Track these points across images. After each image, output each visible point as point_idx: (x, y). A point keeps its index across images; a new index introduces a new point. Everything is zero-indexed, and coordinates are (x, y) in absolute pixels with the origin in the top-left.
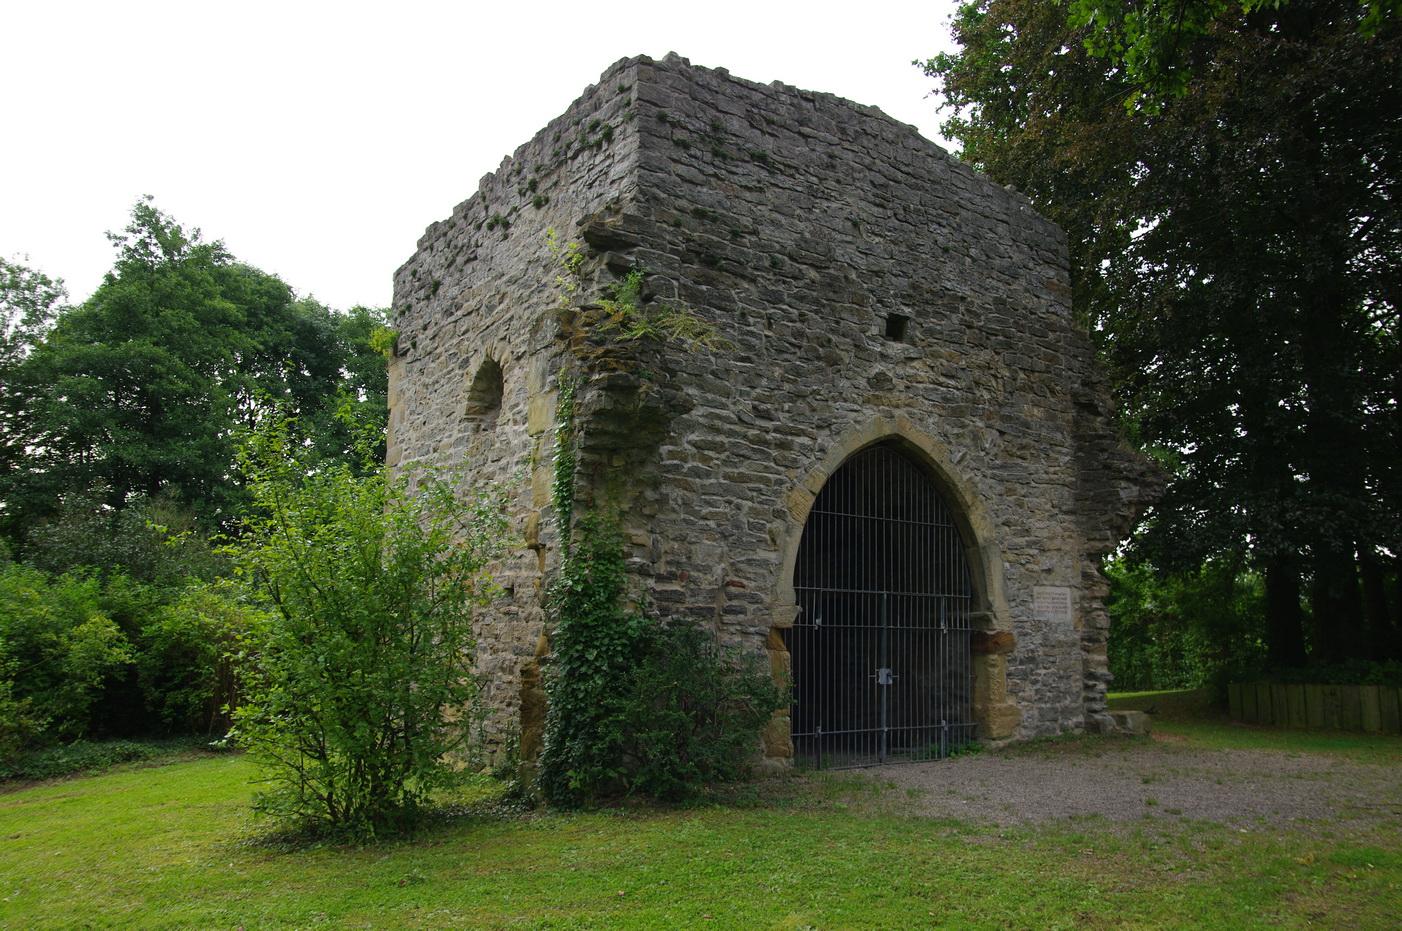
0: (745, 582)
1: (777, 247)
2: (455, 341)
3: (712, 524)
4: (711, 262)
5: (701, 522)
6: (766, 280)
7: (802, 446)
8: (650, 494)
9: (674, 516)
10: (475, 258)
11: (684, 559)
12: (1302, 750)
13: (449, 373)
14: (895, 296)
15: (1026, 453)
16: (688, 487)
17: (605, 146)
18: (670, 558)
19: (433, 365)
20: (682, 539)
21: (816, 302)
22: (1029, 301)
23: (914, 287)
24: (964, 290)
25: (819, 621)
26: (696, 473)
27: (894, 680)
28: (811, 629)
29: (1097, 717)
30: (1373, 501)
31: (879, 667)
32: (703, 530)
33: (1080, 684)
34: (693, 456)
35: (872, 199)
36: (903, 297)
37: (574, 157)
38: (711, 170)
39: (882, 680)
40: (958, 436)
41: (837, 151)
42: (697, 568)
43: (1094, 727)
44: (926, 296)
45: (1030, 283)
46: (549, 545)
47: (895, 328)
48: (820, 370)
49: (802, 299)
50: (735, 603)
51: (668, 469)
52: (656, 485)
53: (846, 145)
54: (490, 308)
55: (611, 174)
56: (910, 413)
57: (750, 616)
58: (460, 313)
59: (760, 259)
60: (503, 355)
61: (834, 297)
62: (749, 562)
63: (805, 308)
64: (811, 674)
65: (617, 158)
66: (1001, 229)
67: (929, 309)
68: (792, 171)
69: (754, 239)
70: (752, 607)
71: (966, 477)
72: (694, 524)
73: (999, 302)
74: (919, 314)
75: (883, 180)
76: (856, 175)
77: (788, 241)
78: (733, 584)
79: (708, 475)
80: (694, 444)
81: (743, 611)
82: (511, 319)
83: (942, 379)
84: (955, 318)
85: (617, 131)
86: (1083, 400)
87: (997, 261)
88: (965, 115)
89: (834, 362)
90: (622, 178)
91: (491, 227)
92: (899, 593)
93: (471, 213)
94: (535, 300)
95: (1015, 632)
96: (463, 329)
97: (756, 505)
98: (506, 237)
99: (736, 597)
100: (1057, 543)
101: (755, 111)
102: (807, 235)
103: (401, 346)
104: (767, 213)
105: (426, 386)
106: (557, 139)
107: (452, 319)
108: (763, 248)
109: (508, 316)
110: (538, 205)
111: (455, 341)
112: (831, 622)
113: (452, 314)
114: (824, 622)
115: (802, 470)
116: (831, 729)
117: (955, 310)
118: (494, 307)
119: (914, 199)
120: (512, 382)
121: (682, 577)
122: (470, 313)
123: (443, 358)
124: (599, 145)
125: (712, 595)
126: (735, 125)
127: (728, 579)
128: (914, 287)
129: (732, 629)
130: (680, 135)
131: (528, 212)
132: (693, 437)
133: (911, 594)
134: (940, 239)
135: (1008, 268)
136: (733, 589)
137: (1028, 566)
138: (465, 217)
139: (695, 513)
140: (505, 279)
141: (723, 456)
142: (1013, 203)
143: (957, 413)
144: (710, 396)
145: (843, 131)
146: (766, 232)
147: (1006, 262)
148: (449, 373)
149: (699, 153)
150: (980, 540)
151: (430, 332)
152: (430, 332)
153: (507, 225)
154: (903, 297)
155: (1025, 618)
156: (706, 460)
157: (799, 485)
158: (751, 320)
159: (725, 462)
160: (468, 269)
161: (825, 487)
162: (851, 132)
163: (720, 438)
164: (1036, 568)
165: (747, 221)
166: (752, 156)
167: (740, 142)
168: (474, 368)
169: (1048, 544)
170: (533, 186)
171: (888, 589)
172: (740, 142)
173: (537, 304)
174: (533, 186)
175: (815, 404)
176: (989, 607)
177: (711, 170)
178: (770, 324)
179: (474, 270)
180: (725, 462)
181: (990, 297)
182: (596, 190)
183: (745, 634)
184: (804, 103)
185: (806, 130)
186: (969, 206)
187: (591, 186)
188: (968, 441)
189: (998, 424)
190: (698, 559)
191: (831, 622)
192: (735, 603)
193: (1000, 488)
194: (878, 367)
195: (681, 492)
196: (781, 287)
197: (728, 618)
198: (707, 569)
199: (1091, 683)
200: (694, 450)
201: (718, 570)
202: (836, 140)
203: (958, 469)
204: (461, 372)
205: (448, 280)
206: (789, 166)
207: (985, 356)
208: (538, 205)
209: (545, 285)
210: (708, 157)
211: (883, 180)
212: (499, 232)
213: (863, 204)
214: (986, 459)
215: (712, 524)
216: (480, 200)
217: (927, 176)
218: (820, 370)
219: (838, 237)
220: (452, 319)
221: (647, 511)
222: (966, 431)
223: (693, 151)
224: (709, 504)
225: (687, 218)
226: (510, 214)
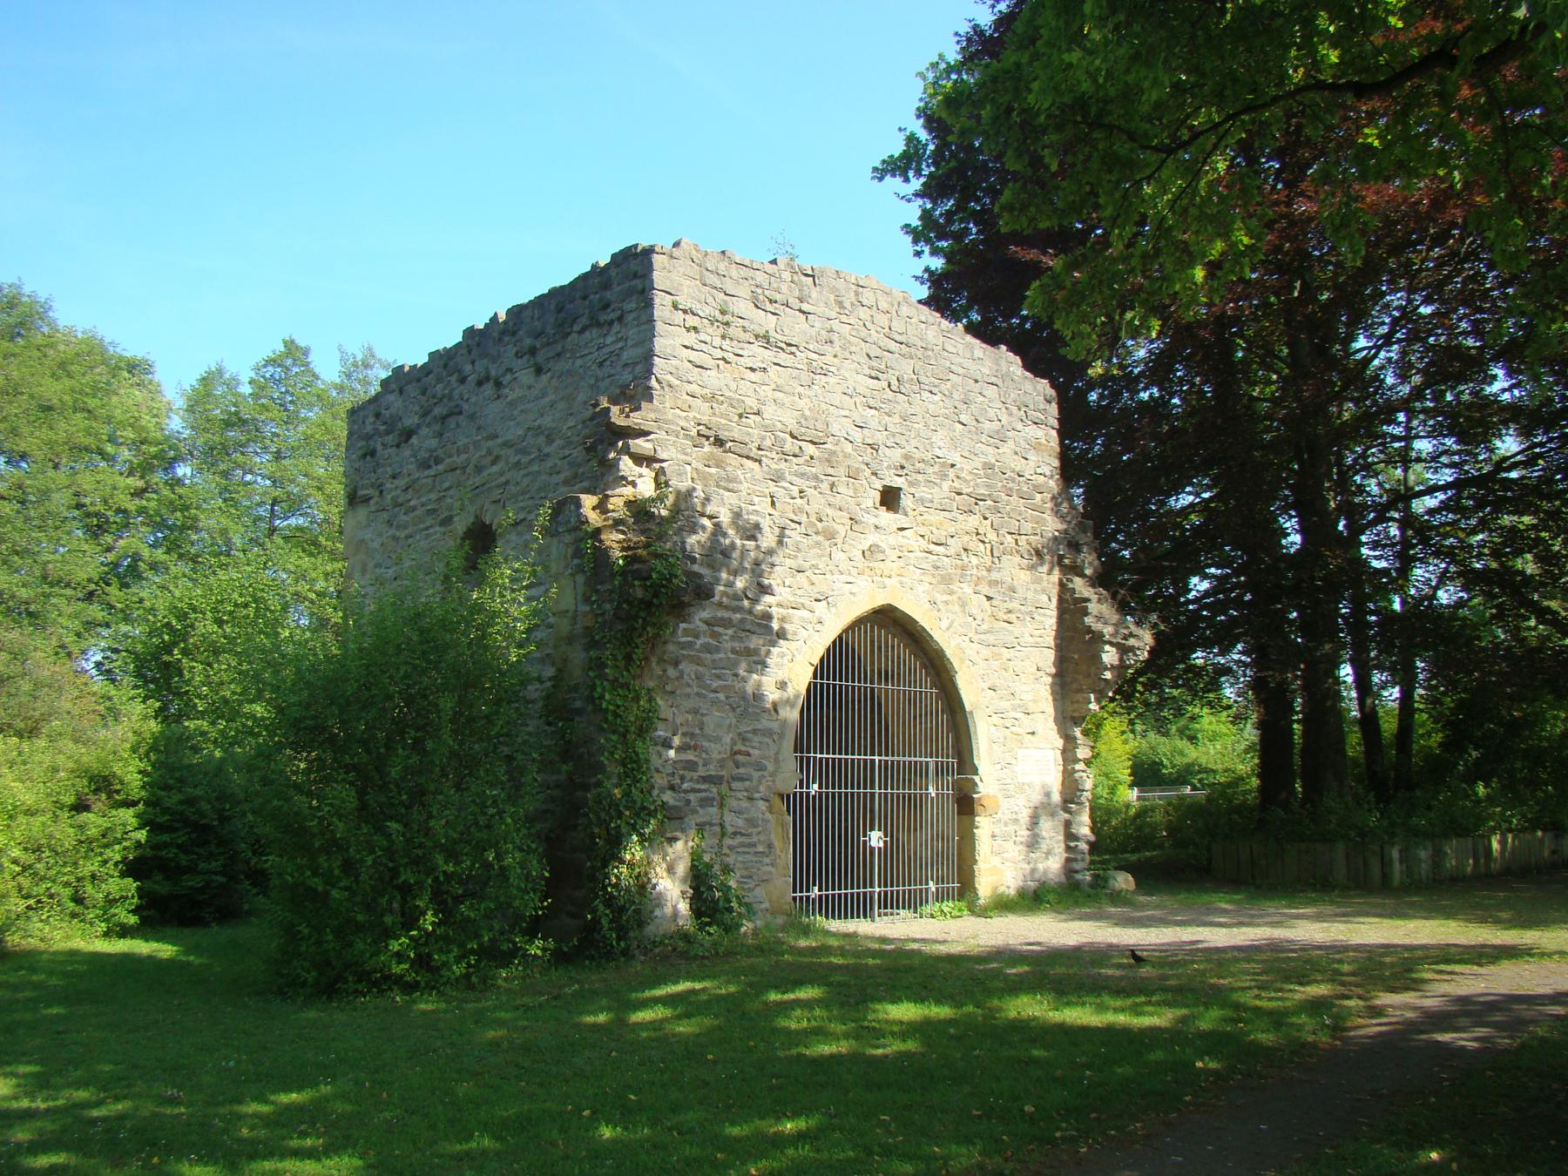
1: (779, 426)
2: (433, 496)
3: (721, 696)
4: (719, 442)
5: (713, 695)
6: (772, 462)
8: (671, 672)
9: (688, 690)
10: (460, 413)
11: (697, 731)
13: (427, 528)
14: (889, 467)
15: (1012, 617)
18: (685, 729)
19: (404, 518)
20: (695, 711)
21: (816, 478)
22: (1019, 464)
23: (907, 457)
24: (955, 457)
25: (816, 786)
26: (708, 649)
31: (872, 829)
32: (714, 702)
35: (868, 372)
37: (581, 332)
38: (719, 354)
39: (874, 843)
40: (946, 602)
41: (835, 324)
45: (1017, 444)
49: (802, 475)
50: (742, 770)
51: (684, 646)
52: (676, 664)
53: (844, 318)
54: (479, 469)
55: (625, 356)
58: (441, 467)
59: (763, 438)
61: (831, 471)
62: (755, 732)
65: (630, 343)
66: (991, 392)
67: (920, 477)
68: (793, 349)
69: (757, 418)
70: (756, 775)
71: (953, 643)
73: (988, 466)
74: (911, 484)
75: (878, 352)
76: (853, 349)
78: (739, 752)
80: (707, 623)
82: (507, 483)
83: (932, 547)
84: (946, 485)
85: (630, 317)
87: (987, 425)
89: (830, 536)
90: (636, 364)
91: (480, 383)
92: (877, 758)
93: (451, 364)
94: (535, 468)
95: (1000, 796)
96: (446, 485)
99: (743, 765)
101: (759, 291)
102: (807, 413)
104: (770, 393)
105: (395, 539)
106: (560, 310)
108: (767, 429)
109: (503, 479)
111: (433, 496)
113: (430, 467)
117: (944, 477)
118: (485, 467)
119: (906, 368)
121: (695, 748)
122: (454, 470)
123: (418, 512)
125: (722, 763)
128: (907, 457)
129: (739, 795)
130: (692, 321)
131: (526, 376)
133: (877, 758)
134: (931, 407)
135: (998, 432)
136: (739, 757)
138: (445, 366)
140: (499, 441)
141: (730, 632)
142: (1003, 363)
143: (946, 580)
145: (840, 304)
146: (769, 411)
147: (996, 426)
148: (427, 528)
149: (708, 339)
151: (401, 482)
152: (401, 482)
153: (498, 385)
156: (715, 635)
157: (798, 658)
158: (756, 500)
161: (822, 660)
162: (847, 305)
163: (726, 614)
164: (1020, 731)
165: (751, 403)
166: (757, 337)
167: (746, 324)
168: (461, 525)
169: (1031, 707)
170: (533, 351)
172: (746, 324)
173: (539, 472)
174: (533, 351)
177: (719, 354)
178: (773, 503)
179: (458, 426)
180: (733, 638)
181: (977, 463)
182: (606, 370)
183: (750, 799)
184: (804, 279)
185: (805, 307)
186: (961, 371)
187: (601, 364)
188: (957, 608)
189: (986, 590)
190: (710, 729)
193: (985, 652)
194: (872, 538)
195: (695, 667)
196: (783, 465)
197: (735, 785)
198: (717, 740)
200: (705, 627)
201: (727, 739)
202: (833, 315)
204: (443, 529)
205: (424, 431)
206: (790, 345)
207: (973, 521)
209: (547, 455)
210: (717, 341)
211: (878, 352)
212: (489, 389)
215: (721, 696)
216: (464, 351)
217: (920, 344)
221: (668, 688)
222: (955, 597)
223: (703, 337)
224: (719, 677)
226: (504, 375)
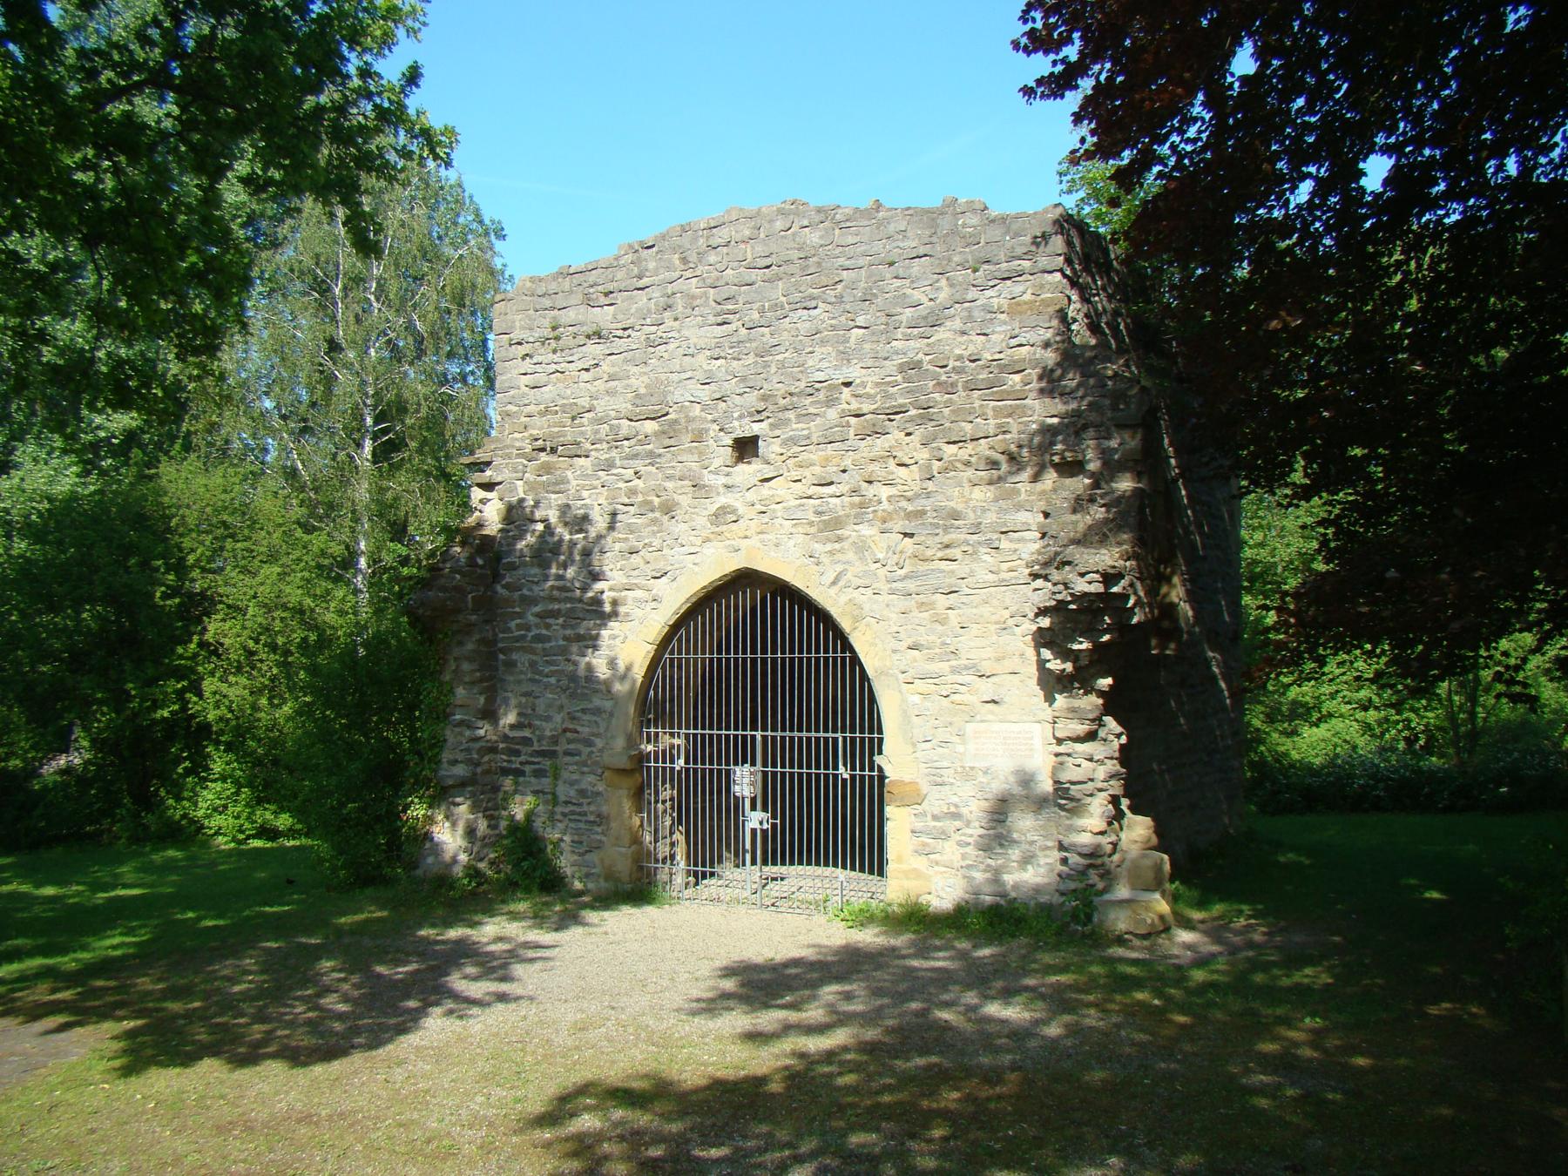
0: (579, 729)
3: (553, 680)
6: (602, 453)
7: (636, 600)
14: (741, 417)
15: (955, 552)
16: (533, 651)
21: (651, 454)
25: (682, 762)
28: (672, 769)
30: (1167, 407)
34: (537, 626)
36: (751, 414)
40: (831, 553)
42: (540, 718)
44: (782, 402)
47: (746, 448)
48: (654, 521)
49: (635, 456)
50: (572, 746)
56: (762, 541)
57: (584, 757)
61: (672, 442)
63: (638, 464)
64: (696, 810)
71: (843, 599)
72: (539, 681)
74: (773, 426)
79: (549, 639)
81: (579, 754)
100: (1009, 665)
112: (695, 762)
114: (687, 762)
115: (636, 623)
116: (696, 865)
121: (530, 726)
125: (555, 740)
128: (764, 398)
132: (537, 609)
137: (953, 697)
139: (540, 673)
141: (561, 621)
146: (601, 405)
154: (751, 414)
155: (945, 764)
156: (548, 626)
157: (630, 637)
159: (564, 627)
171: (843, 731)
175: (648, 556)
180: (564, 627)
190: (540, 710)
191: (695, 762)
192: (572, 746)
198: (548, 719)
203: (833, 591)
218: (654, 521)
219: (675, 377)
222: (846, 544)
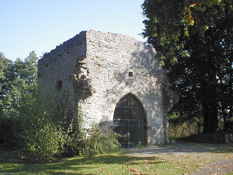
12: (195, 143)
17: (80, 45)
27: (130, 135)
29: (167, 141)
33: (164, 135)
43: (166, 142)
46: (74, 114)
60: (62, 79)
77: (112, 60)
86: (164, 84)
88: (147, 26)
91: (59, 56)
97: (107, 106)
98: (62, 58)
101: (106, 38)
103: (40, 75)
107: (51, 71)
110: (68, 53)
120: (64, 83)
124: (79, 45)
126: (103, 41)
127: (102, 118)
130: (93, 44)
131: (66, 54)
144: (99, 88)
146: (108, 59)
150: (145, 110)
160: (54, 62)
176: (147, 122)
199: (165, 135)
208: (68, 53)
210: (98, 47)
213: (125, 53)
214: (146, 96)
220: (51, 71)
225: (95, 58)
